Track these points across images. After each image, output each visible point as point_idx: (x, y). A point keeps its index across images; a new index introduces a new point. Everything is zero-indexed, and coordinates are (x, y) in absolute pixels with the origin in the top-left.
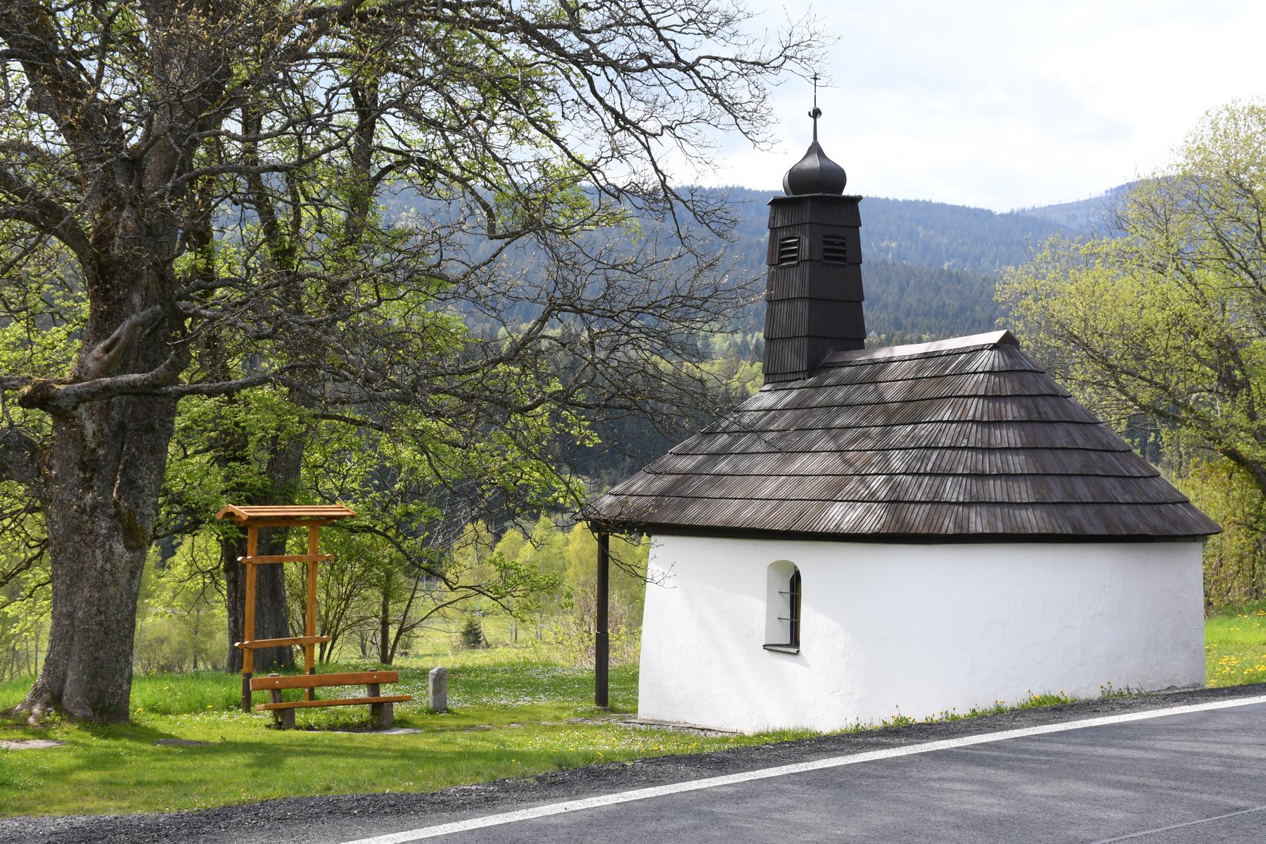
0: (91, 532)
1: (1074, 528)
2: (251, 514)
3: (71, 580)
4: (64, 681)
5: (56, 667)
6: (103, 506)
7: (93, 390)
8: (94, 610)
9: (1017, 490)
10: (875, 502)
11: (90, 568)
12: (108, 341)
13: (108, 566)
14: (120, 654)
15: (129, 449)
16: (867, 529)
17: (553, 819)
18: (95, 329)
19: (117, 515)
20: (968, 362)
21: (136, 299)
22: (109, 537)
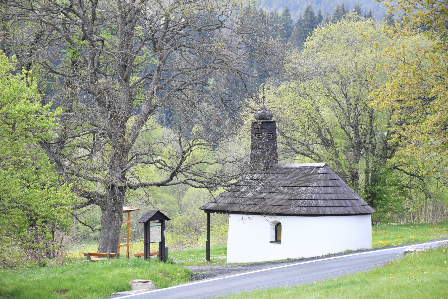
1: (349, 212)
8: (114, 236)
13: (118, 225)
17: (419, 238)
20: (317, 171)
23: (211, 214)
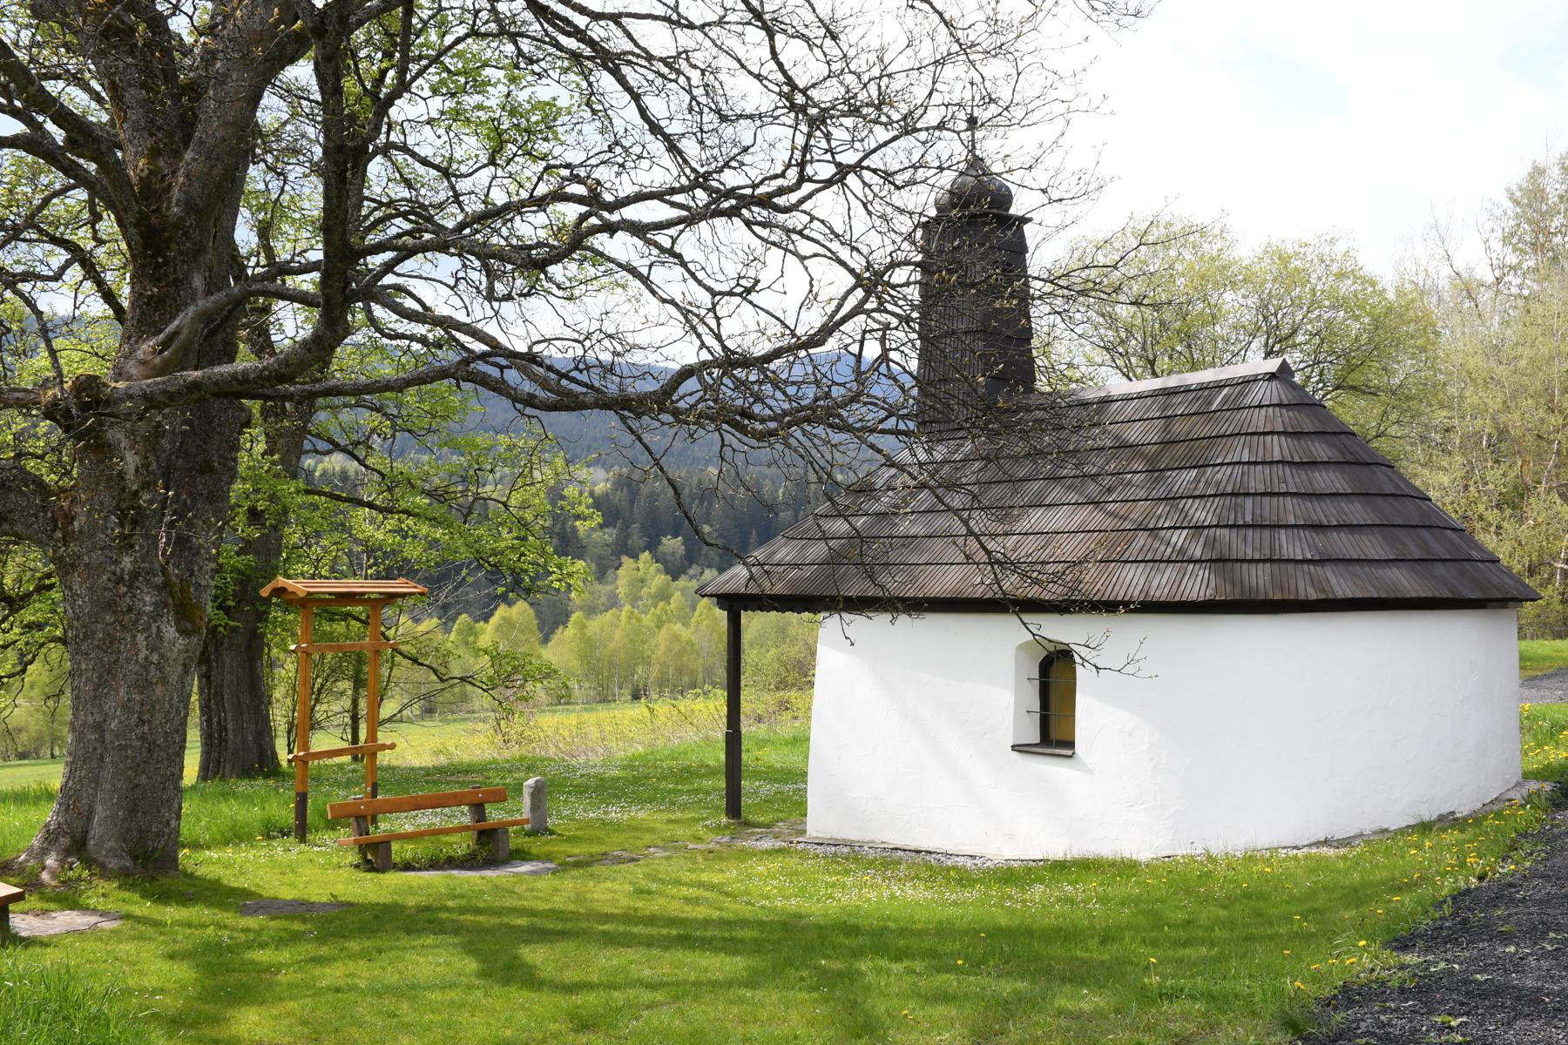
0: (130, 609)
2: (311, 590)
3: (100, 677)
4: (90, 818)
5: (78, 799)
6: (148, 573)
7: (171, 389)
9: (1368, 543)
10: (1189, 561)
11: (127, 661)
12: (161, 337)
13: (155, 657)
14: (167, 779)
15: (177, 495)
16: (1122, 594)
18: (139, 321)
19: (166, 585)
21: (198, 282)
22: (155, 616)
23: (754, 623)
